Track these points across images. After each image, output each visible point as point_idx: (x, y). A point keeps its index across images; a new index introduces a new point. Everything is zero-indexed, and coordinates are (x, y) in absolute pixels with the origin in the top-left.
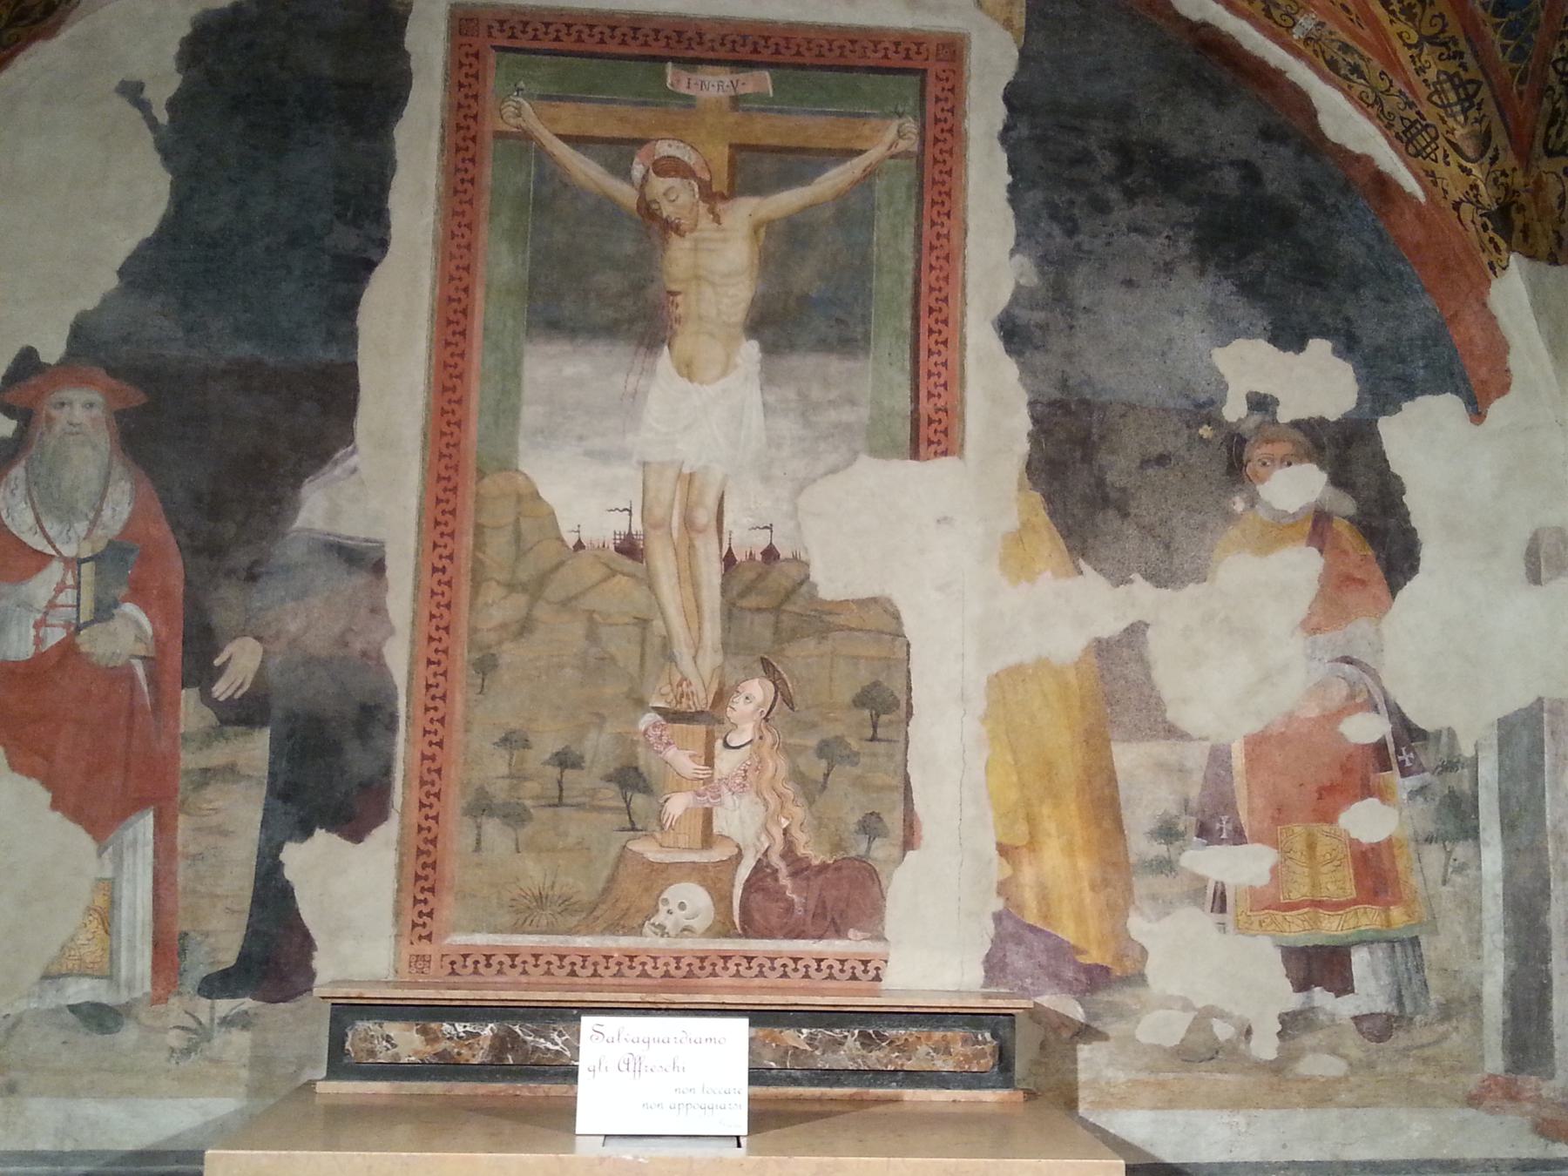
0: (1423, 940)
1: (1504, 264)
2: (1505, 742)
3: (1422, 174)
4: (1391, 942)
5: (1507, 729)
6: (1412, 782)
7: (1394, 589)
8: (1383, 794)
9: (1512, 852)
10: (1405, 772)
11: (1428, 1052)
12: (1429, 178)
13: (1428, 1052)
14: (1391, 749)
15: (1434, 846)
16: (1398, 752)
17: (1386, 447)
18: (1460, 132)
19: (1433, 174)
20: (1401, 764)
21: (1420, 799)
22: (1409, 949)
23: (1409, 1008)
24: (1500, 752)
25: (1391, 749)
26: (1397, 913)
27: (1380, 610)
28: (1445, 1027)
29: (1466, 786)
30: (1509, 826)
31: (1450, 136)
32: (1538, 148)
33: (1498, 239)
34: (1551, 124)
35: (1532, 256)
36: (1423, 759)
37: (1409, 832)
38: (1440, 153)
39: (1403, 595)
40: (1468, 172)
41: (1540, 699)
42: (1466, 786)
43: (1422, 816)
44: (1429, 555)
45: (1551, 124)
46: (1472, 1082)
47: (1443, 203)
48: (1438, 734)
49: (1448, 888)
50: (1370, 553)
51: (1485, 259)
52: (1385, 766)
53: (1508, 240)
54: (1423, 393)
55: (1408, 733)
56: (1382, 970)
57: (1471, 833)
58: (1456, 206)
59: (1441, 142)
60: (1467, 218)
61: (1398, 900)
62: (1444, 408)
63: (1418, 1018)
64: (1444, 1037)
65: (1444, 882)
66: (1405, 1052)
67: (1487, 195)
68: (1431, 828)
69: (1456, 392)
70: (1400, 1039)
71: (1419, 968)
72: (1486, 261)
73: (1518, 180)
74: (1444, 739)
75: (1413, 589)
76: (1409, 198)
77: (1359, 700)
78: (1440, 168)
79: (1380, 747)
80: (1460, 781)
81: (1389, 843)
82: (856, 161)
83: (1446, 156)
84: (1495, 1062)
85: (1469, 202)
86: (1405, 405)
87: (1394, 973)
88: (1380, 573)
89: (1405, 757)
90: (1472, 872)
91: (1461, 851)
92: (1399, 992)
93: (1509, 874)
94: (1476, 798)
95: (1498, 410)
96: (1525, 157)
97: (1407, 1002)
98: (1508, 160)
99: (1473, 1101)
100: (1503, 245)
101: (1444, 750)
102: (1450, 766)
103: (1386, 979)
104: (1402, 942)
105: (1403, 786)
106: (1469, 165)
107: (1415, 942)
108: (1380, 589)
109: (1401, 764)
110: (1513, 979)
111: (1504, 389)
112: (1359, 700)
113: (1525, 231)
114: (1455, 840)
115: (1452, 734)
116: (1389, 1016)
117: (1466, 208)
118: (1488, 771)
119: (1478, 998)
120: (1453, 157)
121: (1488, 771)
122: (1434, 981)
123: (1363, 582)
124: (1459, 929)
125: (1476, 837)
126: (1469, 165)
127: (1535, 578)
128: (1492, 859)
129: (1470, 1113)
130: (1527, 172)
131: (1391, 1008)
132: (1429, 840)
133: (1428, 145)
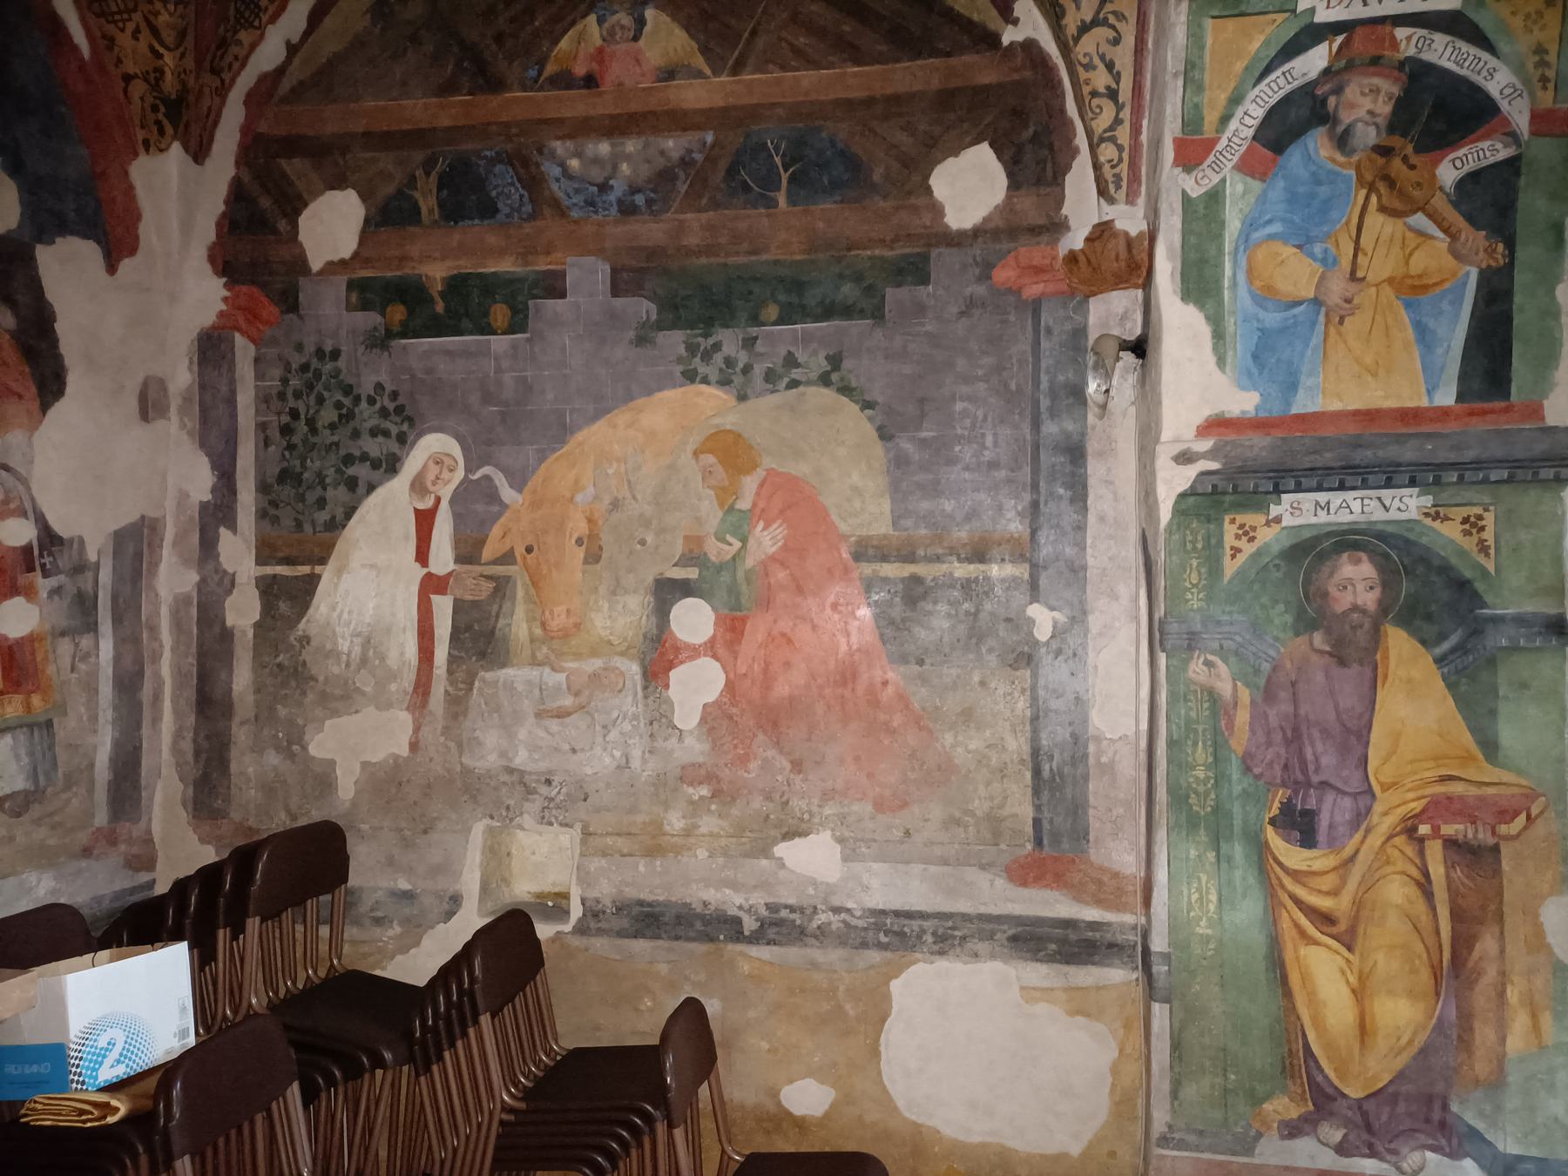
0: (55, 721)
1: (163, 146)
2: (117, 553)
3: (98, 34)
4: (31, 726)
5: (120, 538)
6: (53, 582)
7: (45, 408)
8: (29, 593)
9: (119, 642)
10: (46, 574)
11: (57, 818)
12: (104, 43)
13: (57, 818)
14: (36, 552)
15: (67, 639)
16: (41, 556)
17: (42, 271)
18: (164, 18)
19: (112, 40)
20: (43, 566)
21: (56, 598)
22: (45, 732)
23: (42, 781)
24: (114, 558)
25: (36, 552)
26: (36, 700)
27: (34, 427)
28: (69, 794)
29: (89, 588)
30: (117, 620)
31: (152, 18)
32: (207, 64)
33: (166, 122)
34: (218, 48)
35: (187, 150)
36: (60, 563)
37: (47, 627)
38: (130, 26)
39: (51, 413)
40: (160, 56)
41: (143, 517)
42: (89, 588)
43: (59, 612)
44: (72, 380)
45: (218, 48)
46: (83, 838)
47: (111, 68)
48: (71, 541)
49: (75, 675)
50: (27, 370)
51: (140, 135)
52: (30, 569)
53: (176, 128)
54: (72, 233)
55: (50, 539)
56: (23, 752)
57: (92, 627)
58: (128, 78)
59: (137, 17)
60: (136, 97)
61: (37, 689)
62: (86, 252)
63: (49, 790)
64: (68, 801)
65: (73, 670)
66: (38, 822)
67: (170, 83)
68: (64, 623)
69: (99, 243)
70: (36, 811)
71: (51, 747)
72: (140, 138)
73: (191, 82)
74: (75, 546)
75: (59, 409)
76: (75, 49)
77: (12, 506)
78: (124, 40)
79: (27, 549)
80: (86, 583)
81: (31, 639)
82: (994, 12)
83: (137, 31)
84: (101, 818)
85: (146, 80)
86: (58, 240)
87: (31, 754)
88: (34, 389)
89: (47, 560)
90: (92, 659)
91: (86, 642)
92: (35, 769)
93: (117, 659)
94: (96, 597)
95: (126, 265)
96: (199, 63)
97: (42, 779)
98: (189, 62)
99: (87, 852)
100: (169, 130)
101: (75, 553)
102: (80, 568)
103: (25, 760)
104: (39, 725)
105: (44, 585)
106: (162, 50)
107: (49, 724)
108: (35, 406)
109: (43, 566)
110: (117, 744)
111: (132, 251)
112: (12, 506)
113: (187, 126)
114: (81, 633)
115: (81, 541)
116: (26, 793)
117: (138, 88)
118: (105, 576)
119: (92, 766)
120: (145, 35)
121: (105, 576)
122: (62, 756)
123: (20, 397)
124: (83, 710)
125: (96, 631)
126: (162, 50)
127: (145, 416)
128: (106, 648)
129: (84, 863)
130: (197, 78)
131: (29, 786)
132: (63, 634)
133: (120, 12)
